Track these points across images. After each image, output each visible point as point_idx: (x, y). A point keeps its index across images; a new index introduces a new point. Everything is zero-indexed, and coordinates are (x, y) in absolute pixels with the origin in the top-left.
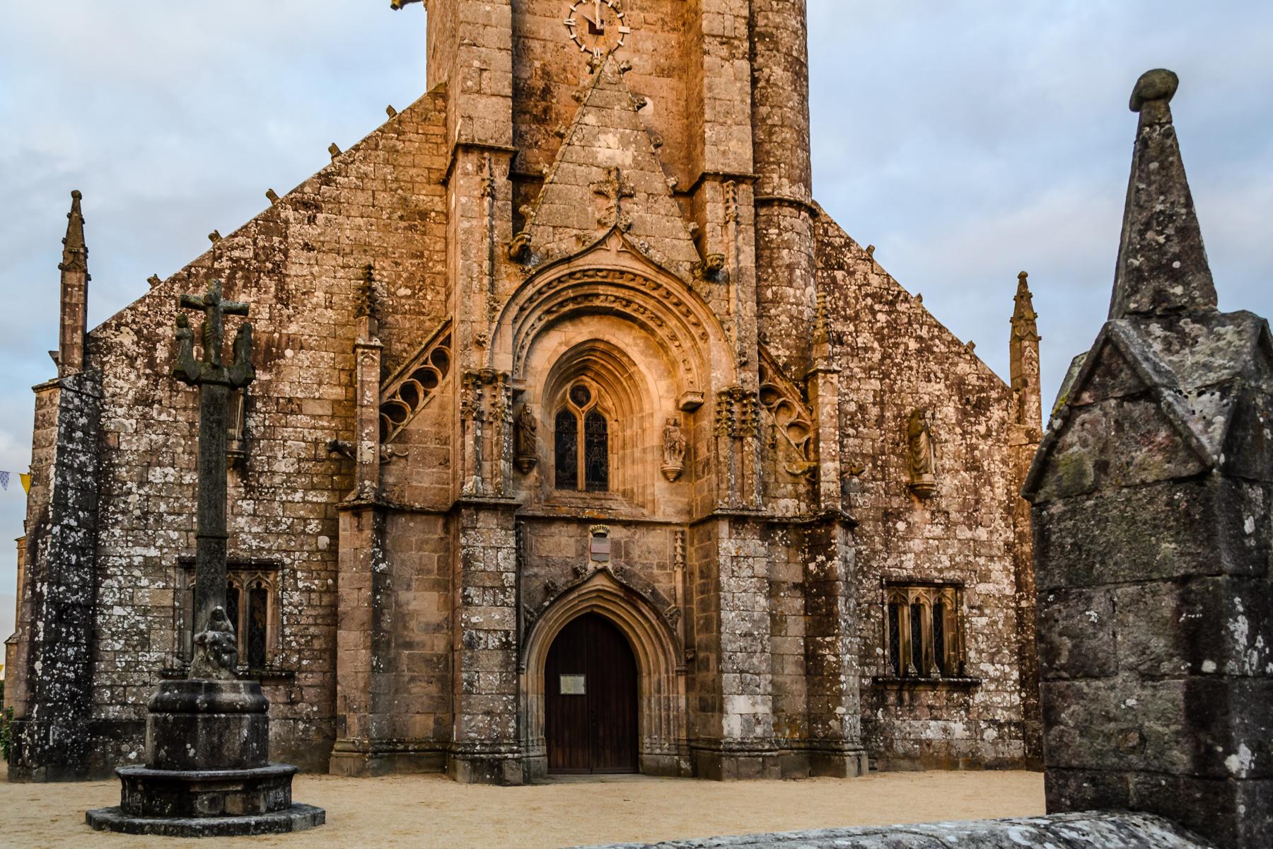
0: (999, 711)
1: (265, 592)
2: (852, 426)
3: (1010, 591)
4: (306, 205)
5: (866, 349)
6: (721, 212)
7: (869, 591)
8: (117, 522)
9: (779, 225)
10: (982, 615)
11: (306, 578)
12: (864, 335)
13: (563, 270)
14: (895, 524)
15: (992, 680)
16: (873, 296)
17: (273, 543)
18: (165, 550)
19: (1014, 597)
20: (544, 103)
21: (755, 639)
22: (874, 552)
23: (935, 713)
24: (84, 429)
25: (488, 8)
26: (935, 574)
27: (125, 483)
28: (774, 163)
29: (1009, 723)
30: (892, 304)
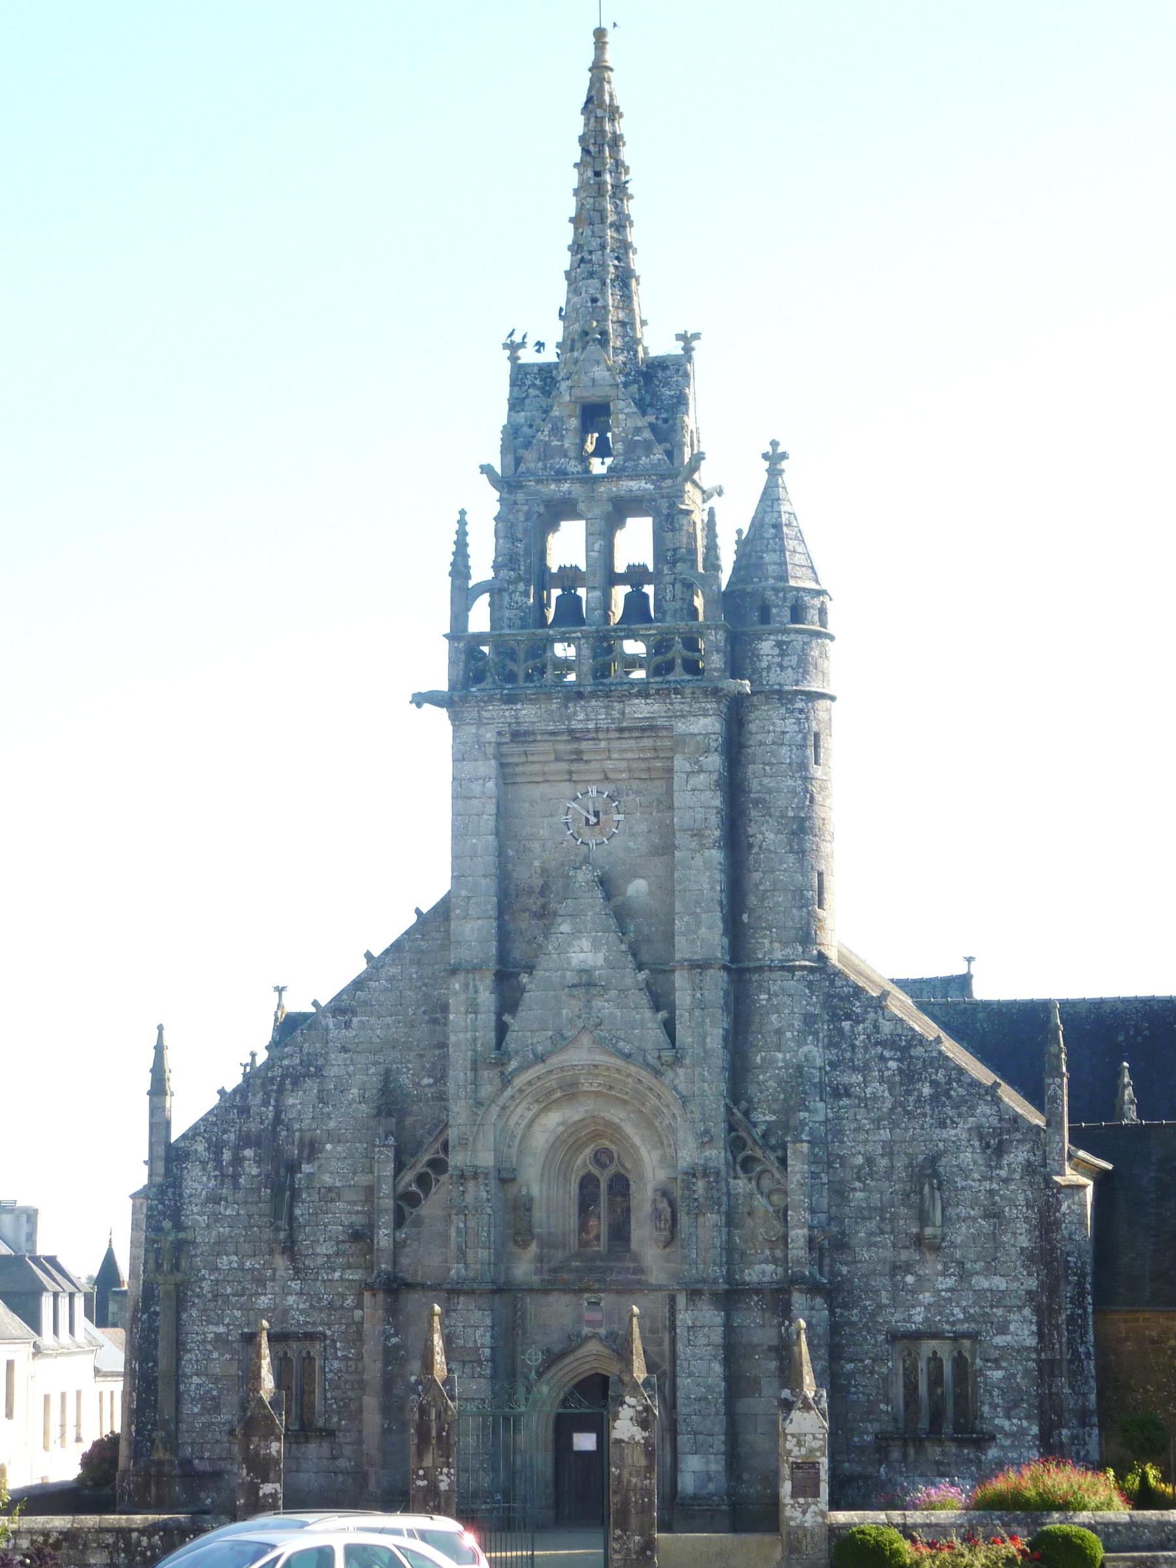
2: (859, 1179)
3: (1031, 1342)
4: (343, 1011)
6: (688, 999)
9: (769, 990)
10: (999, 1368)
12: (874, 1085)
14: (903, 1278)
15: (1007, 1435)
16: (883, 1044)
17: (317, 1317)
18: (231, 1327)
20: (542, 900)
21: (710, 1403)
23: (942, 1468)
25: (474, 841)
26: (947, 1327)
27: (199, 1271)
28: (765, 928)
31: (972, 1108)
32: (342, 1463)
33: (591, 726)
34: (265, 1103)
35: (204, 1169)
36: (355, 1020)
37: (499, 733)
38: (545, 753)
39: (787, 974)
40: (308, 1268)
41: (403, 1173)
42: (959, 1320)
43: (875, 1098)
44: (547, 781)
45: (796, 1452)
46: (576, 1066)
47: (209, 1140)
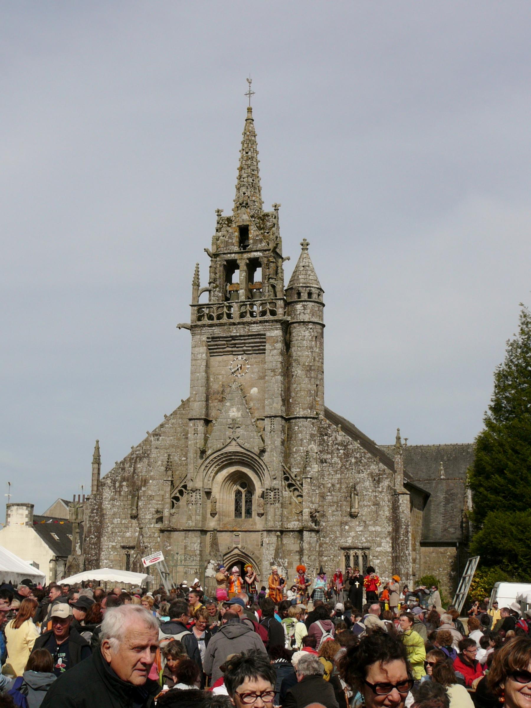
2: (329, 492)
3: (390, 550)
4: (157, 435)
5: (335, 464)
6: (269, 428)
7: (334, 551)
8: (105, 535)
10: (378, 559)
13: (219, 453)
16: (338, 444)
22: (337, 537)
24: (97, 509)
26: (360, 544)
31: (369, 466)
34: (130, 466)
36: (160, 438)
47: (112, 479)
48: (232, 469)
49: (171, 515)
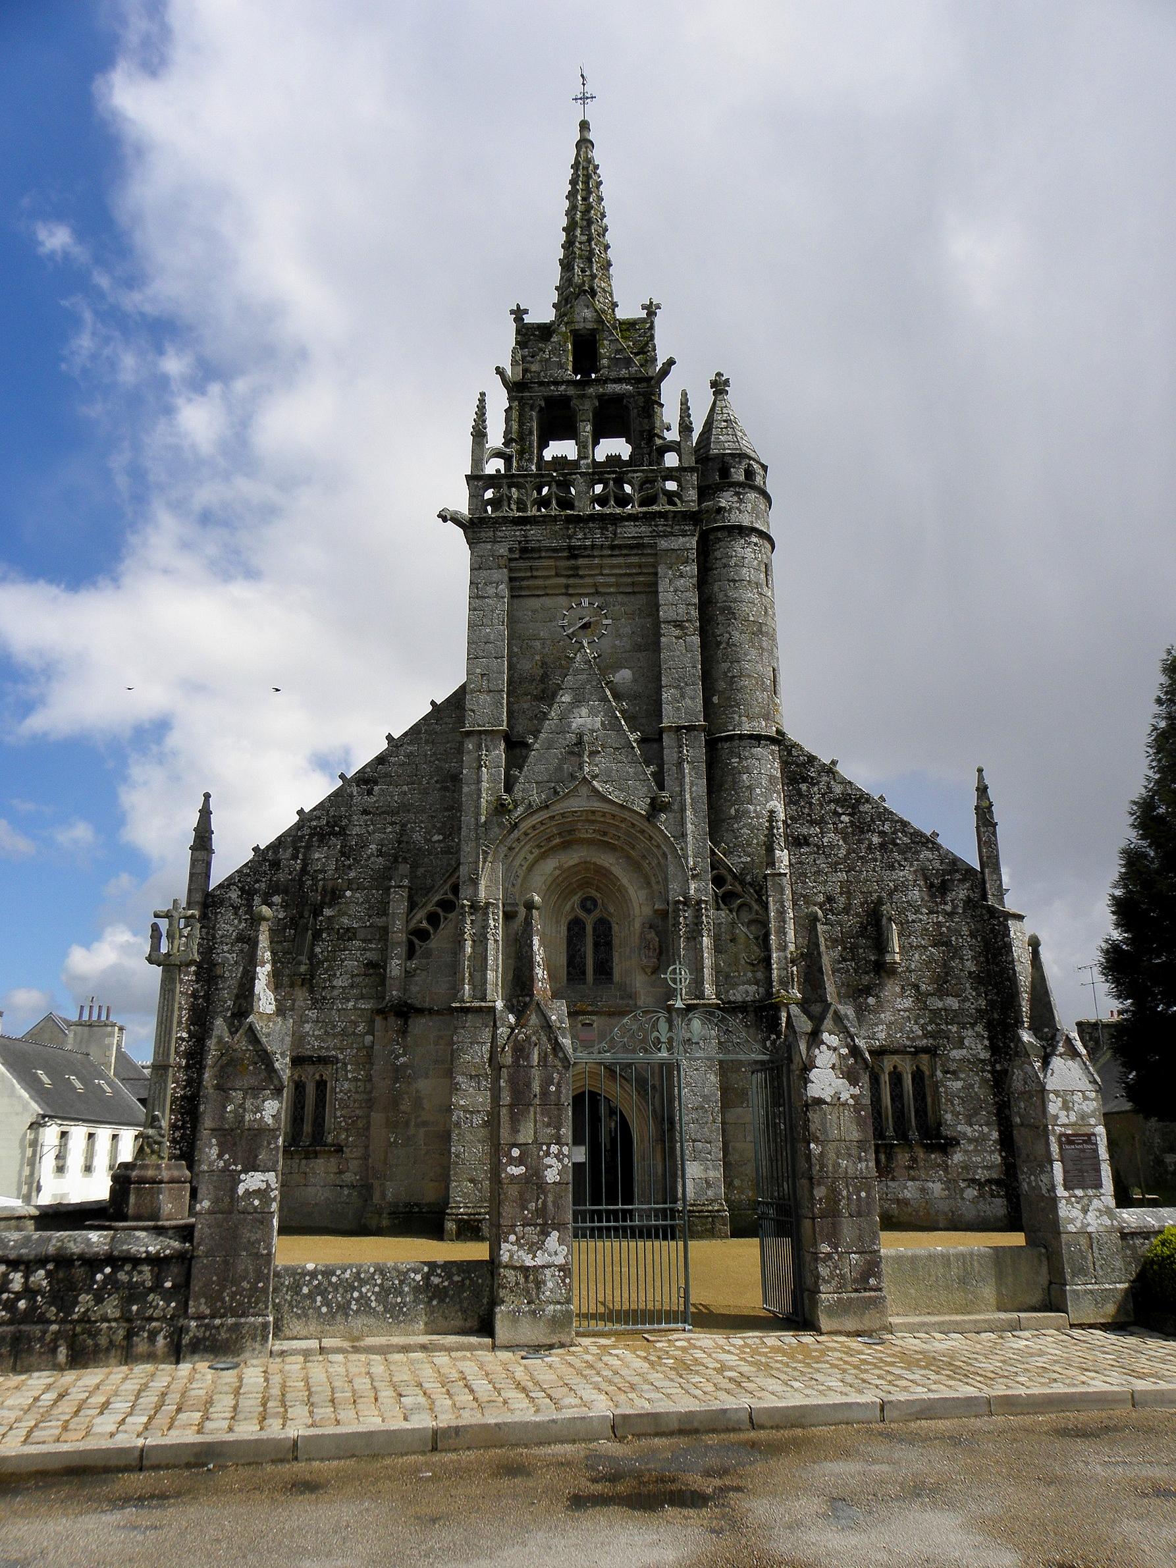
0: (979, 1171)
1: (326, 1082)
3: (985, 1055)
4: (366, 781)
5: (831, 846)
10: (958, 1079)
11: (355, 1070)
15: (970, 1141)
16: (837, 801)
17: (331, 1042)
19: (989, 1060)
20: (543, 686)
21: (706, 1111)
26: (908, 1043)
27: (225, 1002)
29: (989, 1181)
30: (854, 807)
31: (917, 853)
32: (349, 1177)
33: (588, 543)
34: (295, 857)
35: (236, 914)
37: (511, 550)
38: (548, 568)
39: (753, 741)
40: (324, 998)
41: (415, 911)
42: (918, 1036)
43: (832, 847)
44: (548, 595)
45: (1063, 1120)
46: (576, 812)
47: (242, 889)
48: (572, 858)
49: (409, 974)
